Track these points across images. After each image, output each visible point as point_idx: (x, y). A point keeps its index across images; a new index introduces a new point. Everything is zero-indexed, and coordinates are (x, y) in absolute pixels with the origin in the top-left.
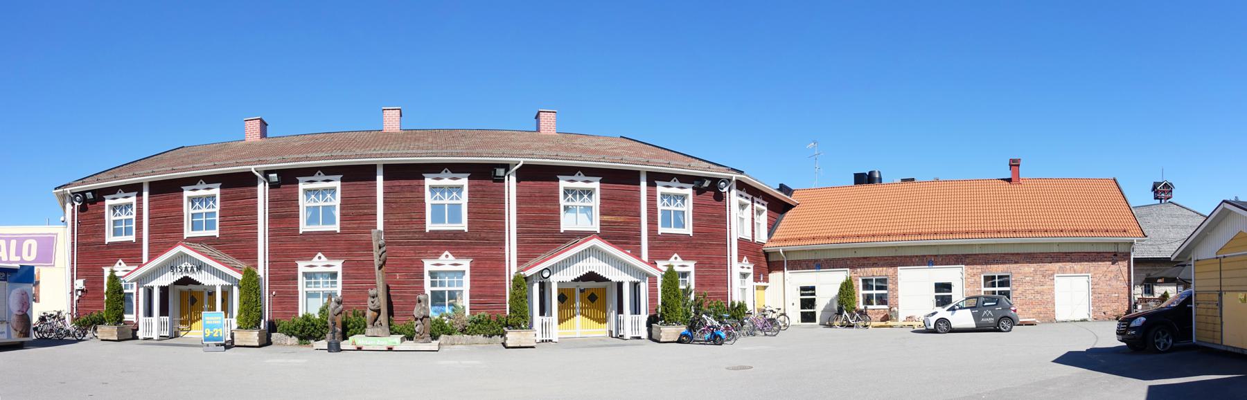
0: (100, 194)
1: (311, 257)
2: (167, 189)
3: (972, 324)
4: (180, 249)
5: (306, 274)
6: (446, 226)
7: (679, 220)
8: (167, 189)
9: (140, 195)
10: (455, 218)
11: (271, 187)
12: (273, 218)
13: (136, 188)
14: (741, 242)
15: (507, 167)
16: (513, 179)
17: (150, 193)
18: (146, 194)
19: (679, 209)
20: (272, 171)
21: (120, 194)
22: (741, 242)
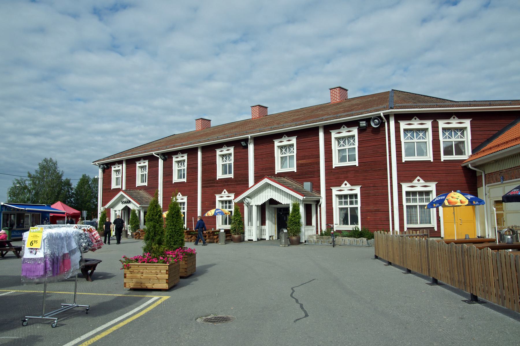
1: (220, 193)
4: (266, 180)
12: (164, 168)
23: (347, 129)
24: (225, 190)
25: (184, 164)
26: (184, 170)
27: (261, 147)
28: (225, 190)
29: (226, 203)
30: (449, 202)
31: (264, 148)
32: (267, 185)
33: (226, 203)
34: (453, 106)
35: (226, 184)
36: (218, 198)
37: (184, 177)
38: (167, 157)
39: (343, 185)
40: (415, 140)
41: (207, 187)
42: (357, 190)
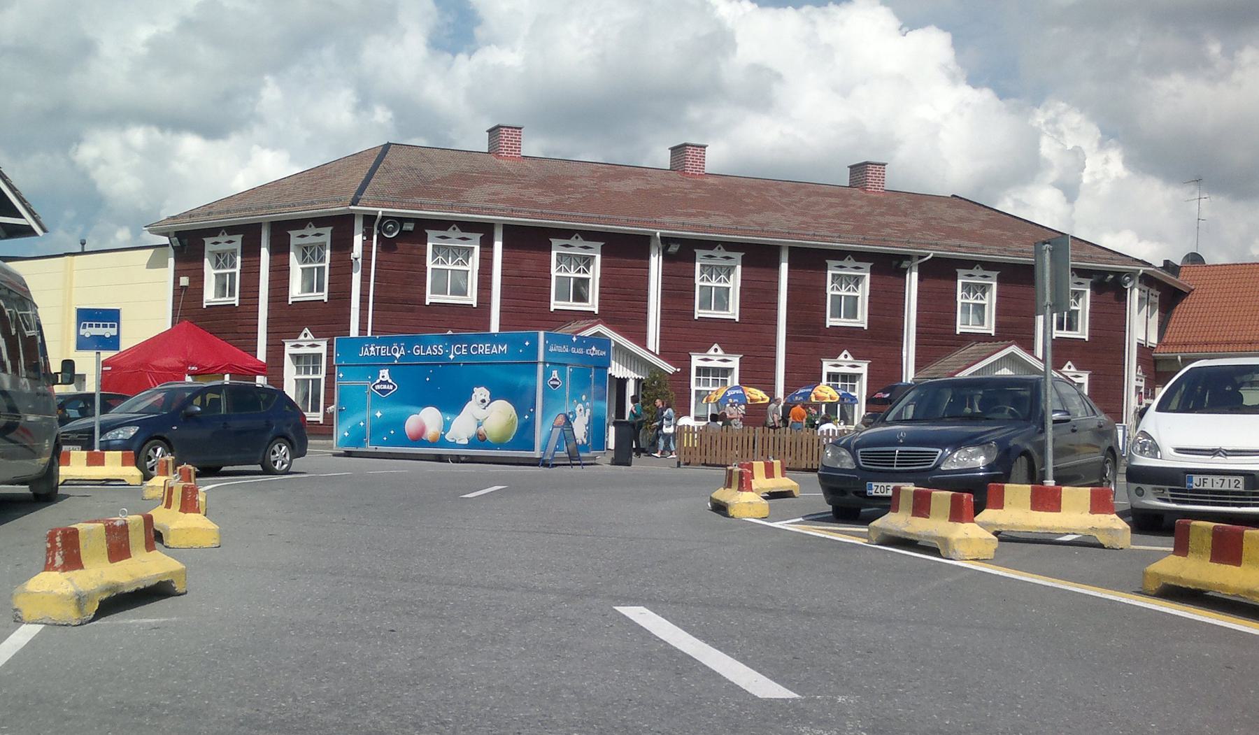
0: (424, 225)
1: (295, 336)
2: (529, 241)
3: (79, 250)
5: (698, 369)
6: (842, 322)
7: (722, 298)
8: (529, 241)
9: (487, 245)
10: (723, 304)
11: (385, 244)
12: (272, 270)
13: (486, 231)
14: (1143, 349)
15: (908, 257)
16: (915, 275)
17: (505, 246)
18: (498, 246)
19: (582, 275)
20: (409, 220)
21: (978, 271)
22: (1143, 349)
23: (981, 272)
24: (306, 330)
25: (231, 260)
26: (233, 275)
27: (752, 269)
28: (306, 330)
29: (307, 362)
30: (817, 398)
31: (529, 260)
32: (1012, 356)
33: (307, 362)
34: (1097, 260)
35: (848, 339)
36: (827, 367)
37: (232, 294)
38: (185, 241)
39: (711, 352)
40: (450, 266)
41: (799, 339)
42: (863, 368)
